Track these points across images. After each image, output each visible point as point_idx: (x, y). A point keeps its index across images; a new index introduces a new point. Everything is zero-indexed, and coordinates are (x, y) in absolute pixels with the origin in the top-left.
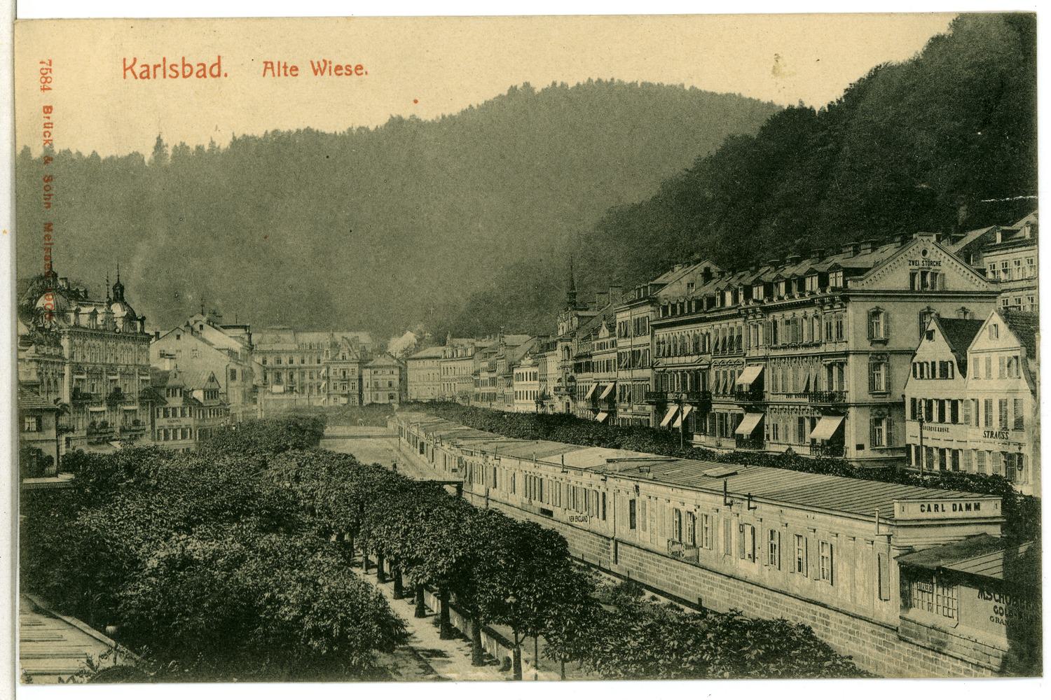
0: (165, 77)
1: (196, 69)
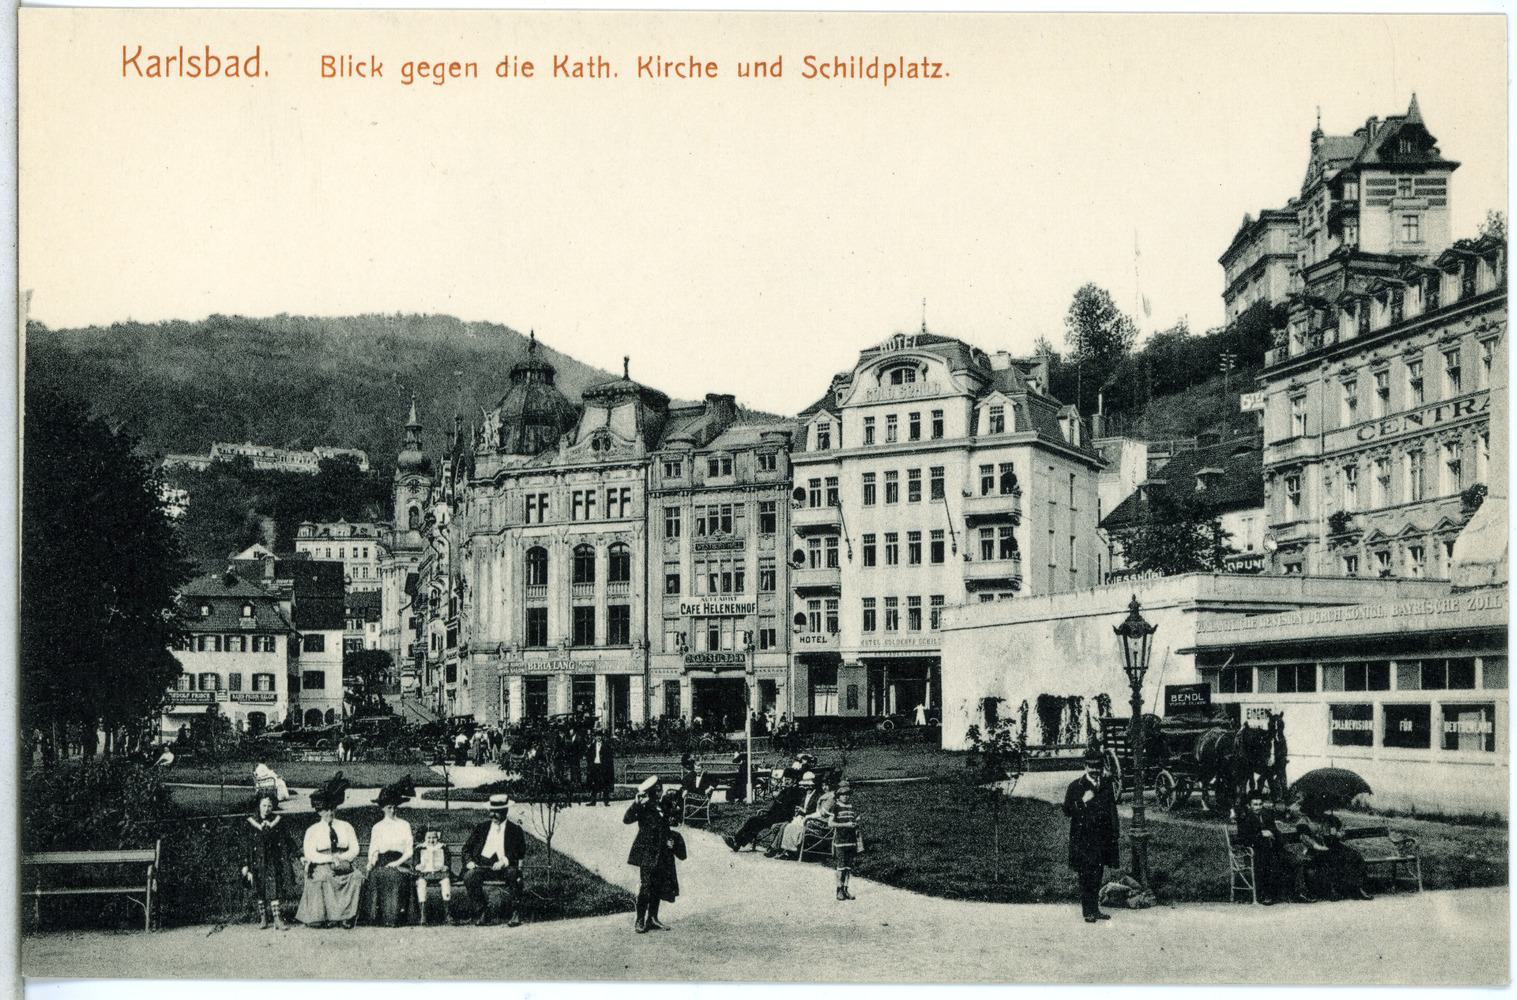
1: (225, 64)
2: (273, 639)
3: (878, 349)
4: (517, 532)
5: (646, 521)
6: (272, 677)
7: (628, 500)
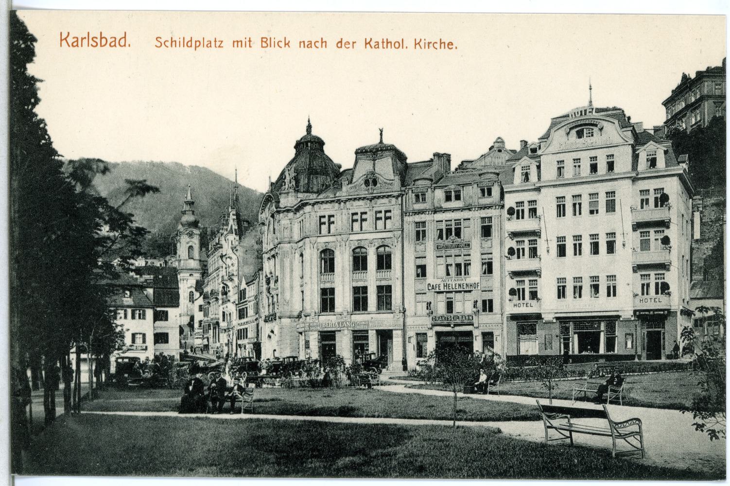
2: (144, 312)
3: (567, 116)
4: (313, 239)
5: (402, 231)
6: (144, 335)
7: (333, 222)
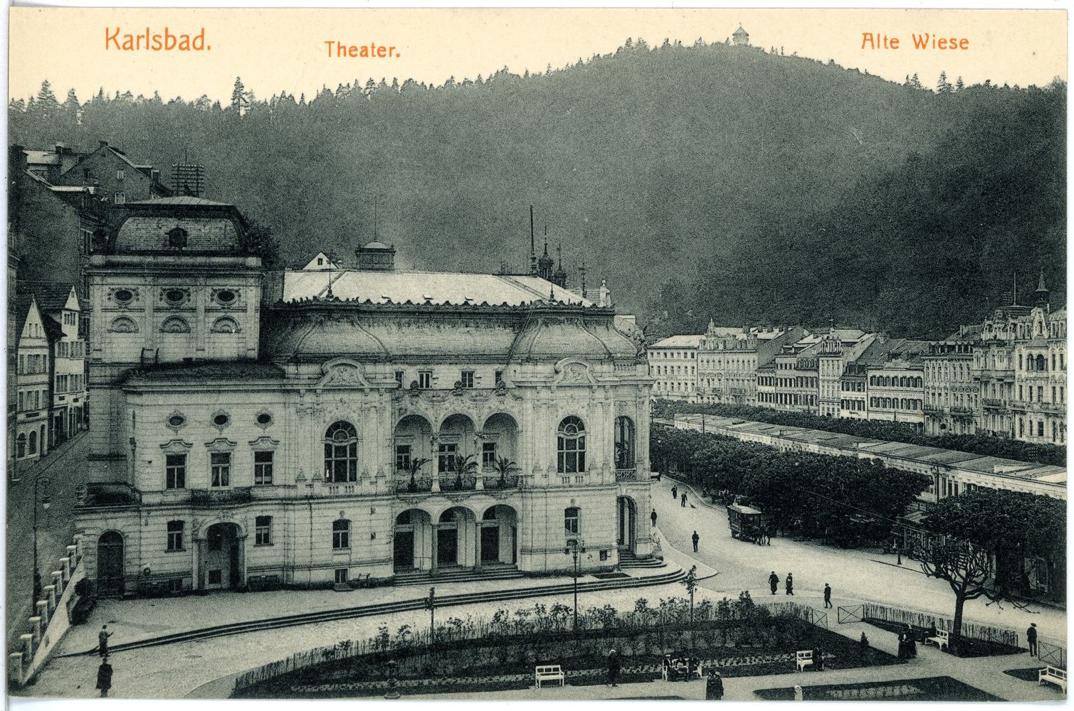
0: (148, 48)
1: (179, 41)
